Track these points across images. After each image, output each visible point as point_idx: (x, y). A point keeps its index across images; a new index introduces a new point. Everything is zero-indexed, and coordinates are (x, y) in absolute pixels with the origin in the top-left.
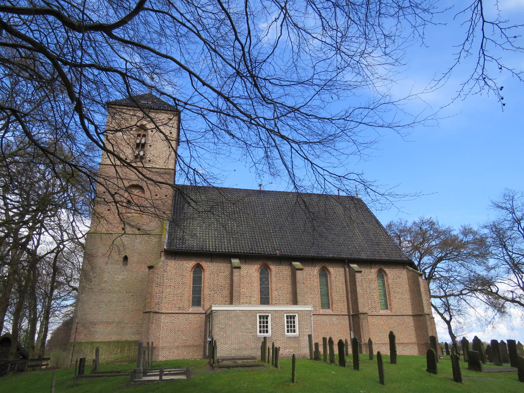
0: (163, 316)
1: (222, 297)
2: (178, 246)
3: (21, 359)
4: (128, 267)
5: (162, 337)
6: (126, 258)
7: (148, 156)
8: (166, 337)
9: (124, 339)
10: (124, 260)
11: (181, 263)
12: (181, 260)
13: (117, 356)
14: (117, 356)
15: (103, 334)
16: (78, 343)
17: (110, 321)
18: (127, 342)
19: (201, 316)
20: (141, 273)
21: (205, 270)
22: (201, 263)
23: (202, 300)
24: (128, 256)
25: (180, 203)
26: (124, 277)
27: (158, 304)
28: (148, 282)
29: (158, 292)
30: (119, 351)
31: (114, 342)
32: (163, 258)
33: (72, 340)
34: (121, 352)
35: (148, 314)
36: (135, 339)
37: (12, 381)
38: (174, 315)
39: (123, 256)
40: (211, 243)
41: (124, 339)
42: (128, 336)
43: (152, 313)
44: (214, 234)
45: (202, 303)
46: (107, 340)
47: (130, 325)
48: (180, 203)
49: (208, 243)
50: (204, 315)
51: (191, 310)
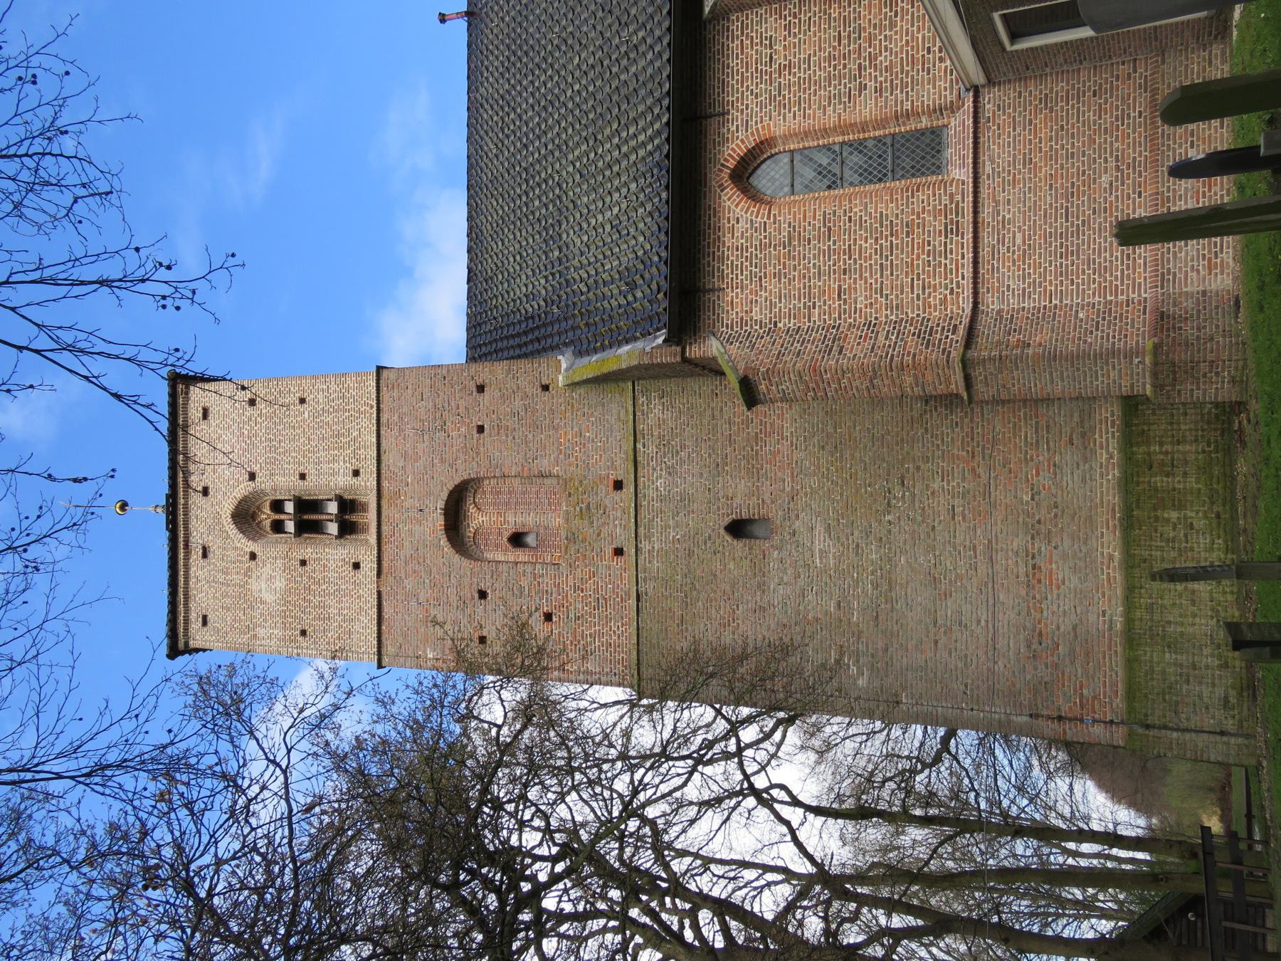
0: (991, 303)
1: (892, 25)
2: (652, 291)
3: (1196, 915)
4: (776, 515)
5: (1102, 291)
6: (738, 529)
7: (342, 481)
8: (1102, 270)
9: (1114, 498)
10: (750, 536)
11: (732, 257)
12: (721, 259)
13: (1200, 524)
14: (1200, 524)
15: (1087, 587)
16: (1131, 710)
17: (1022, 570)
18: (1127, 484)
19: (988, 107)
20: (798, 455)
21: (764, 134)
22: (731, 164)
23: (911, 126)
24: (727, 520)
25: (525, 333)
26: (819, 529)
27: (926, 335)
28: (821, 391)
29: (868, 345)
30: (1174, 515)
31: (1128, 543)
32: (712, 347)
33: (1119, 736)
34: (1180, 506)
35: (978, 373)
36: (1114, 446)
37: (1280, 928)
38: (985, 252)
39: (728, 538)
40: (642, 138)
41: (1114, 498)
42: (1097, 478)
43: (970, 354)
44: (610, 138)
45: (925, 122)
46: (1118, 576)
47: (1045, 479)
48: (525, 333)
49: (642, 153)
50: (989, 101)
51: (960, 173)
